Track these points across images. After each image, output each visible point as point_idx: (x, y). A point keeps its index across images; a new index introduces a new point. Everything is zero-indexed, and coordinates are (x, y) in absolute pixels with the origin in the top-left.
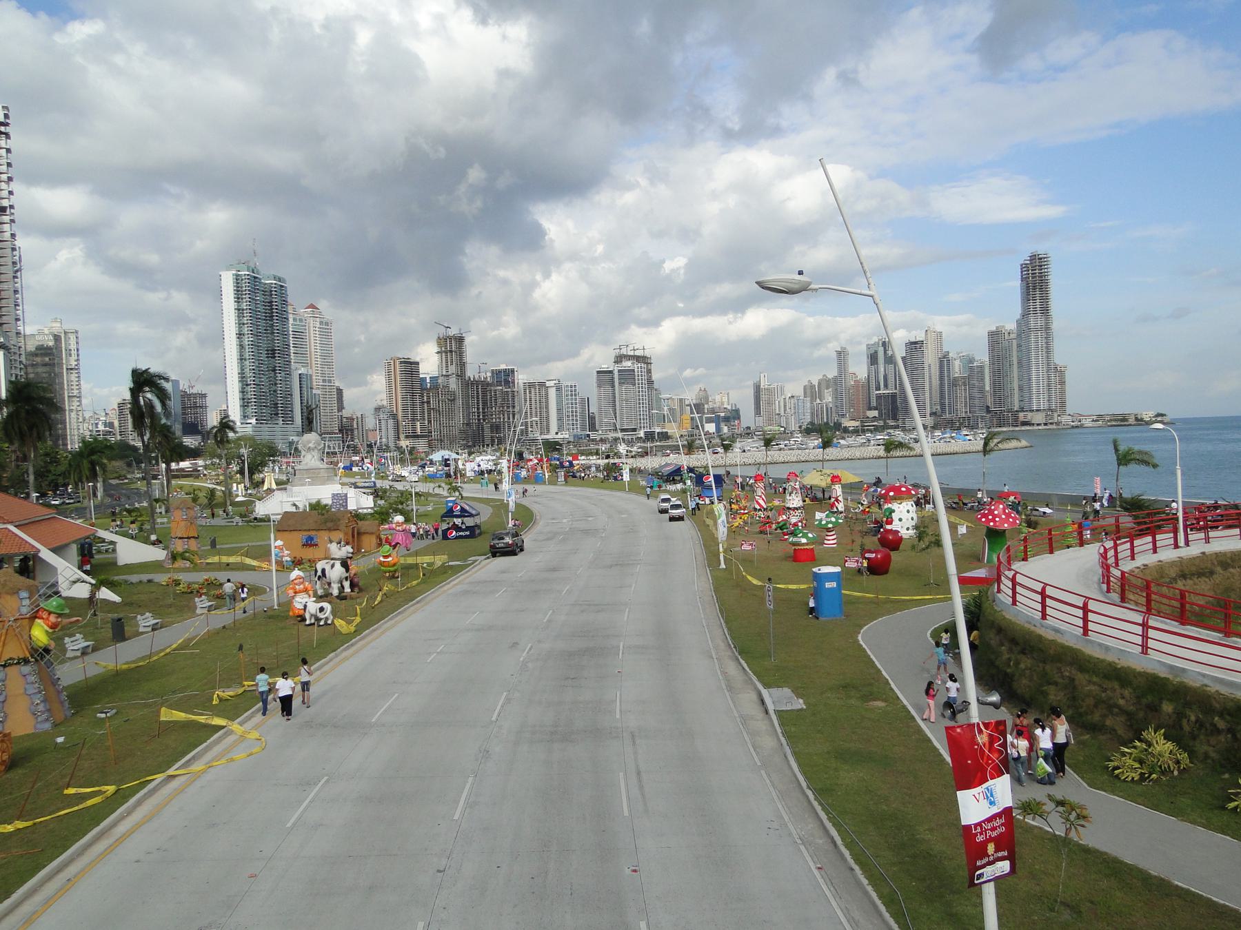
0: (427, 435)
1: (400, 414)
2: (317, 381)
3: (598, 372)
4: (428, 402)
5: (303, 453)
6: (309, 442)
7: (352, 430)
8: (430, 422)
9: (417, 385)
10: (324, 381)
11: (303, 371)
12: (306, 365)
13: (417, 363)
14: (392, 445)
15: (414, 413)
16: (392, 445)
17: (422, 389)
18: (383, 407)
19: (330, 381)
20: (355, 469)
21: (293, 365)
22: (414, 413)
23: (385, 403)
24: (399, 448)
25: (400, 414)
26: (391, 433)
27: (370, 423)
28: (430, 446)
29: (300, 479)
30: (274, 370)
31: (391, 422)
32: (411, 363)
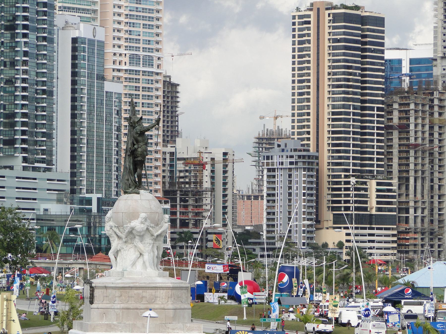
0: (393, 217)
1: (325, 156)
2: (116, 59)
3: (23, 170)
4: (404, 128)
5: (115, 244)
6: (134, 215)
7: (198, 195)
8: (404, 181)
9: (376, 81)
10: (134, 59)
11: (83, 31)
12: (89, 14)
13: (380, 21)
14: (299, 239)
15: (362, 156)
16: (299, 239)
17: (389, 92)
18: (280, 135)
19: (149, 61)
20: (211, 297)
21: (60, 18)
22: (362, 156)
23: (286, 125)
24: (317, 250)
25: (325, 156)
26: (299, 204)
27: (245, 176)
28: (401, 247)
29: (105, 312)
30: (12, 28)
31: (300, 177)
32: (363, 20)
